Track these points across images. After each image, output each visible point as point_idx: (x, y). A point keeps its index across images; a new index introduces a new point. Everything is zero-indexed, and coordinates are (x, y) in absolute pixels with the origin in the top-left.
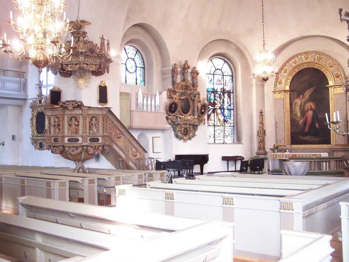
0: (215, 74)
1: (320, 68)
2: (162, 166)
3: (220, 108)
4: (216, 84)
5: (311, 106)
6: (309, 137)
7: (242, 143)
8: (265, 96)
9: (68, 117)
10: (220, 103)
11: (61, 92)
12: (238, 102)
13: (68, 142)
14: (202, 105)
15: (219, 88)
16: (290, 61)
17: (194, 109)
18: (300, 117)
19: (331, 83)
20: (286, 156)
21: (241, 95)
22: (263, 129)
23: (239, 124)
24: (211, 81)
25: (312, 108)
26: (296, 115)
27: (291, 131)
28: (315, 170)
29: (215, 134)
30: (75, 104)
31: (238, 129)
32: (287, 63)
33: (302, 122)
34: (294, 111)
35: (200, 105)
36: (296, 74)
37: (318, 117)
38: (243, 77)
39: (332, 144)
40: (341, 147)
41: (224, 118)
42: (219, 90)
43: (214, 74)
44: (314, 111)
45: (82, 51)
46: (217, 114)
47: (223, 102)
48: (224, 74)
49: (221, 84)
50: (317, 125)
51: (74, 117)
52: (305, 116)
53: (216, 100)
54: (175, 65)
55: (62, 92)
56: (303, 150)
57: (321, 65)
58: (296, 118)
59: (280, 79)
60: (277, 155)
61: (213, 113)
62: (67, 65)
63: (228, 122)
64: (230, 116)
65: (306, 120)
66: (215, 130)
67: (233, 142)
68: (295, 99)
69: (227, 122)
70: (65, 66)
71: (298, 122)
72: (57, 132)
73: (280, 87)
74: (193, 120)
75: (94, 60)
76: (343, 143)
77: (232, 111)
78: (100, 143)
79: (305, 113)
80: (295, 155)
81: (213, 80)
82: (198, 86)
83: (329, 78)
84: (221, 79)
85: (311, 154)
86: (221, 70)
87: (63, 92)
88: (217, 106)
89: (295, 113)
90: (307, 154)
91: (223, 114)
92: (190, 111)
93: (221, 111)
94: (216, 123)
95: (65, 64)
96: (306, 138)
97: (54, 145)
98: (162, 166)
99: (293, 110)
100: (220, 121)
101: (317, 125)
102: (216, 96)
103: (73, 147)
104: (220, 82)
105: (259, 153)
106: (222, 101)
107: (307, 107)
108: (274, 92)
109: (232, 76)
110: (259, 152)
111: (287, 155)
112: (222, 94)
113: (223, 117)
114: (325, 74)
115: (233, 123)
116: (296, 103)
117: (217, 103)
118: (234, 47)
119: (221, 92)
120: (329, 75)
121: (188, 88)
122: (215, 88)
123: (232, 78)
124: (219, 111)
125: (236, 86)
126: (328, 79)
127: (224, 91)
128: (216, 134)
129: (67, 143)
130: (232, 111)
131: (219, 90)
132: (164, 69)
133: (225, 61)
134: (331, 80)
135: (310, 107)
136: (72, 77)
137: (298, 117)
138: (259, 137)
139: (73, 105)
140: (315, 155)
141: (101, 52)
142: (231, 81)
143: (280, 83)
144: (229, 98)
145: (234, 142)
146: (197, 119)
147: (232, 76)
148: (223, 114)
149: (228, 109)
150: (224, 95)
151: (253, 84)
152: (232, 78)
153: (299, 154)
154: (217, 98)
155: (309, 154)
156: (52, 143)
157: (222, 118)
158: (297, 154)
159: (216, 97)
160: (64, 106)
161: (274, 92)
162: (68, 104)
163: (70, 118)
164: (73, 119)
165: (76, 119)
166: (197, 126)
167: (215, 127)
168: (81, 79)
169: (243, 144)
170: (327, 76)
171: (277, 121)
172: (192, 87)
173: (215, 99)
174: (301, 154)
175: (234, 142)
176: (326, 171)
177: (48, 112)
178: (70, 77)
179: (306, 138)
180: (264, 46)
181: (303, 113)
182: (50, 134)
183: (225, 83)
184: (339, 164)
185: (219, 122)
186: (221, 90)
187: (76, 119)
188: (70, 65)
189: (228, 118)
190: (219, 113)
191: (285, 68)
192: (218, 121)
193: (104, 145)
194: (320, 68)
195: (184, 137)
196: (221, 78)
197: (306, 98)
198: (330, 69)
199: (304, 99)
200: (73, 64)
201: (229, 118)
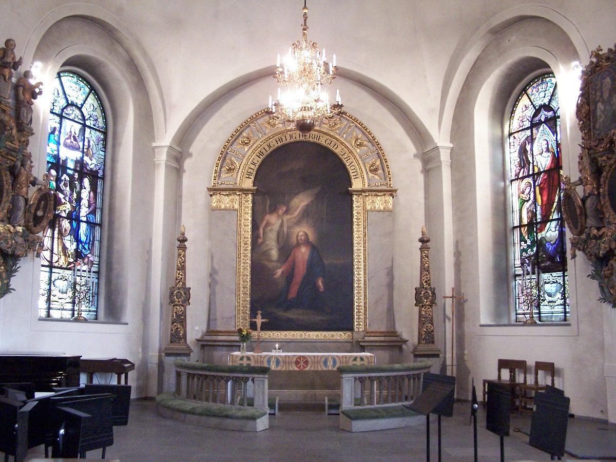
0: (64, 115)
1: (332, 144)
2: (62, 431)
3: (70, 217)
4: (66, 145)
5: (306, 234)
6: (300, 311)
7: (124, 321)
8: (184, 199)
10: (70, 202)
12: (117, 203)
14: (42, 193)
15: (70, 156)
16: (259, 119)
17: (14, 202)
18: (278, 261)
19: (357, 185)
20: (278, 362)
21: (130, 187)
22: (184, 284)
23: (116, 266)
24: (53, 132)
25: (309, 239)
26: (266, 254)
27: (251, 296)
28: (371, 403)
29: (50, 290)
31: (114, 281)
32: (252, 123)
33: (283, 272)
34: (262, 243)
35: (32, 193)
36: (271, 153)
37: (323, 263)
38: (137, 139)
39: (356, 330)
40: (382, 339)
41: (78, 245)
42: (71, 165)
43: (61, 116)
44: (314, 248)
46: (60, 233)
47: (79, 199)
48: (88, 123)
49: (78, 149)
50: (320, 283)
52: (290, 259)
53: (62, 192)
56: (284, 343)
57: (336, 139)
58: (267, 263)
59: (231, 160)
60: (252, 358)
61: (50, 227)
63: (86, 260)
64: (93, 244)
65: (293, 269)
66: (53, 279)
67: (93, 317)
68: (264, 213)
69: (83, 259)
71: (272, 272)
73: (227, 179)
74: (12, 239)
76: (383, 329)
77: (97, 228)
79: (292, 250)
80: (304, 357)
81: (57, 133)
82: (33, 134)
83: (354, 171)
84: (77, 135)
85: (351, 356)
86: (80, 109)
88: (62, 208)
89: (264, 248)
90: (337, 356)
91: (75, 233)
93: (71, 223)
94: (55, 258)
96: (291, 315)
98: (62, 431)
99: (260, 241)
100: (65, 255)
101: (320, 283)
102: (63, 178)
104: (74, 142)
105: (175, 352)
106: (75, 195)
107: (297, 237)
108: (214, 191)
109: (105, 133)
110: (172, 349)
111: (281, 359)
112: (76, 176)
113: (75, 244)
114: (345, 161)
115: (99, 265)
116: (268, 224)
117: (63, 201)
118: (125, 54)
119: (75, 170)
120: (355, 163)
121: (5, 130)
122: (62, 157)
123: (105, 140)
124: (66, 224)
125: (114, 161)
126: (351, 174)
127: (82, 169)
128: (55, 291)
130: (97, 228)
131: (71, 165)
133: (92, 89)
134: (357, 176)
135: (303, 238)
137: (272, 261)
138: (174, 306)
140: (358, 359)
142: (101, 146)
143: (230, 170)
144: (93, 192)
145: (96, 319)
146: (21, 237)
147: (105, 133)
148: (75, 233)
149: (87, 222)
150: (81, 180)
151: (159, 165)
152: (105, 140)
153: (314, 356)
154: (65, 185)
155: (343, 356)
157: (72, 247)
158: (309, 356)
159: (63, 183)
161: (214, 191)
166: (15, 258)
167: (54, 270)
169: (127, 324)
170: (348, 167)
171: (216, 266)
172: (14, 131)
173: (58, 188)
174: (322, 357)
175: (96, 319)
176: (120, 385)
179: (291, 315)
180: (304, 29)
181: (286, 250)
183: (88, 149)
184: (409, 386)
185: (63, 257)
186: (76, 166)
189: (86, 247)
190: (66, 230)
191: (244, 134)
192: (61, 254)
194: (332, 144)
196: (77, 133)
197: (293, 214)
198: (358, 151)
199: (288, 217)
201: (89, 248)
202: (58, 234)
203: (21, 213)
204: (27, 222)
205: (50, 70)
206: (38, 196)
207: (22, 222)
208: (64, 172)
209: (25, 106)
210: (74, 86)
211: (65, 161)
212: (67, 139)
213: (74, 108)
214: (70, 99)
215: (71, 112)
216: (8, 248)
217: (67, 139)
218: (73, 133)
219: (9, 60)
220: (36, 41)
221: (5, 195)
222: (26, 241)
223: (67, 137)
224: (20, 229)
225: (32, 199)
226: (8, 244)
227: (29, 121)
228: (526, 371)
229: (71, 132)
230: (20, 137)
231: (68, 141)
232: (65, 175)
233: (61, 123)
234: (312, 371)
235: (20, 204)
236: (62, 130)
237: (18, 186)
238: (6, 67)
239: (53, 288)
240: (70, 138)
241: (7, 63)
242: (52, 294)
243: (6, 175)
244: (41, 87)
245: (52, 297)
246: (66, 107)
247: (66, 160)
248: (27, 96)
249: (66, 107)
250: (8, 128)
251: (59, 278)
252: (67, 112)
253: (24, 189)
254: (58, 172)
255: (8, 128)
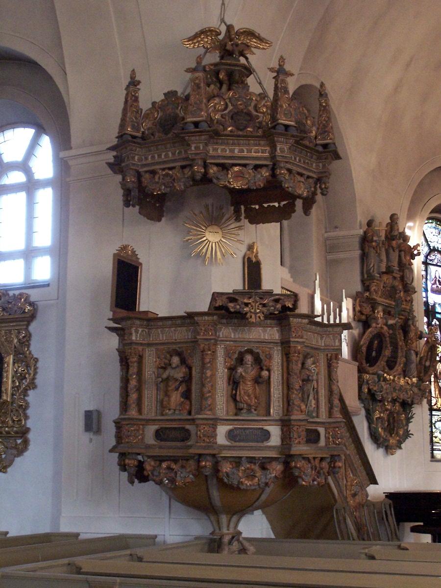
4: (433, 291)
9: (228, 355)
11: (138, 267)
13: (155, 443)
17: (408, 357)
30: (271, 304)
45: (287, 123)
51: (250, 351)
54: (370, 223)
55: (141, 268)
62: (224, 167)
66: (433, 422)
70: (215, 168)
72: (173, 405)
75: (304, 162)
78: (321, 449)
82: (415, 292)
87: (143, 266)
92: (400, 364)
95: (217, 165)
97: (157, 452)
102: (433, 323)
103: (251, 460)
129: (224, 447)
132: (332, 234)
136: (163, 219)
139: (264, 305)
141: (324, 139)
156: (148, 447)
160: (232, 310)
162: (246, 301)
163: (236, 356)
164: (249, 358)
165: (257, 360)
167: (434, 413)
168: (209, 229)
177: (137, 332)
178: (159, 220)
182: (140, 411)
187: (257, 360)
188: (236, 169)
193: (332, 456)
195: (390, 440)
200: (245, 165)
202: (434, 377)
203: (413, 366)
204: (419, 372)
205: (418, 226)
206: (427, 349)
207: (415, 374)
208: (434, 317)
209: (408, 268)
210: (434, 230)
211: (434, 306)
212: (433, 284)
213: (436, 252)
214: (432, 245)
215: (434, 257)
216: (408, 398)
217: (433, 284)
218: (438, 278)
219: (396, 233)
220: (406, 204)
221: (399, 351)
222: (420, 389)
223: (433, 282)
224: (414, 380)
225: (423, 352)
226: (408, 394)
227: (411, 281)
228: (216, 512)
229: (435, 277)
230: (406, 297)
231: (434, 286)
232: (435, 320)
233: (426, 270)
234: (181, 97)
235: (412, 357)
236: (428, 277)
237: (409, 342)
238: (394, 240)
239: (434, 430)
240: (435, 283)
241: (394, 236)
242: (434, 435)
243: (400, 334)
244: (419, 248)
245: (434, 438)
246: (429, 254)
247: (435, 304)
248: (408, 258)
249: (429, 254)
250: (398, 292)
251: (439, 420)
252: (431, 258)
253: (414, 344)
254: (428, 318)
255: (398, 292)
